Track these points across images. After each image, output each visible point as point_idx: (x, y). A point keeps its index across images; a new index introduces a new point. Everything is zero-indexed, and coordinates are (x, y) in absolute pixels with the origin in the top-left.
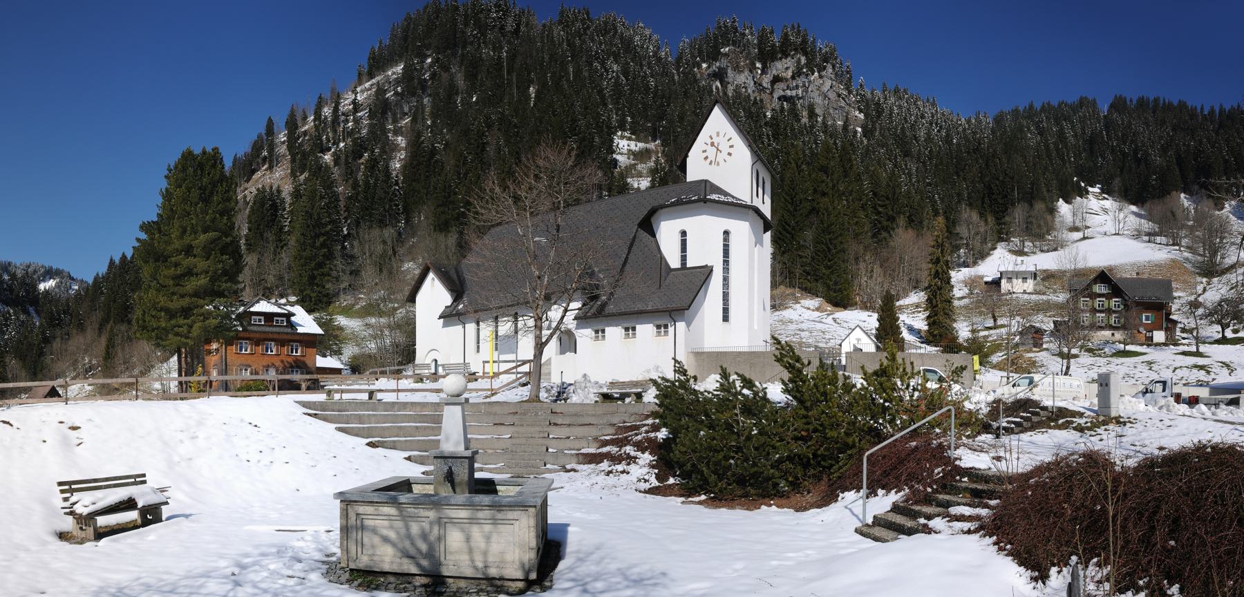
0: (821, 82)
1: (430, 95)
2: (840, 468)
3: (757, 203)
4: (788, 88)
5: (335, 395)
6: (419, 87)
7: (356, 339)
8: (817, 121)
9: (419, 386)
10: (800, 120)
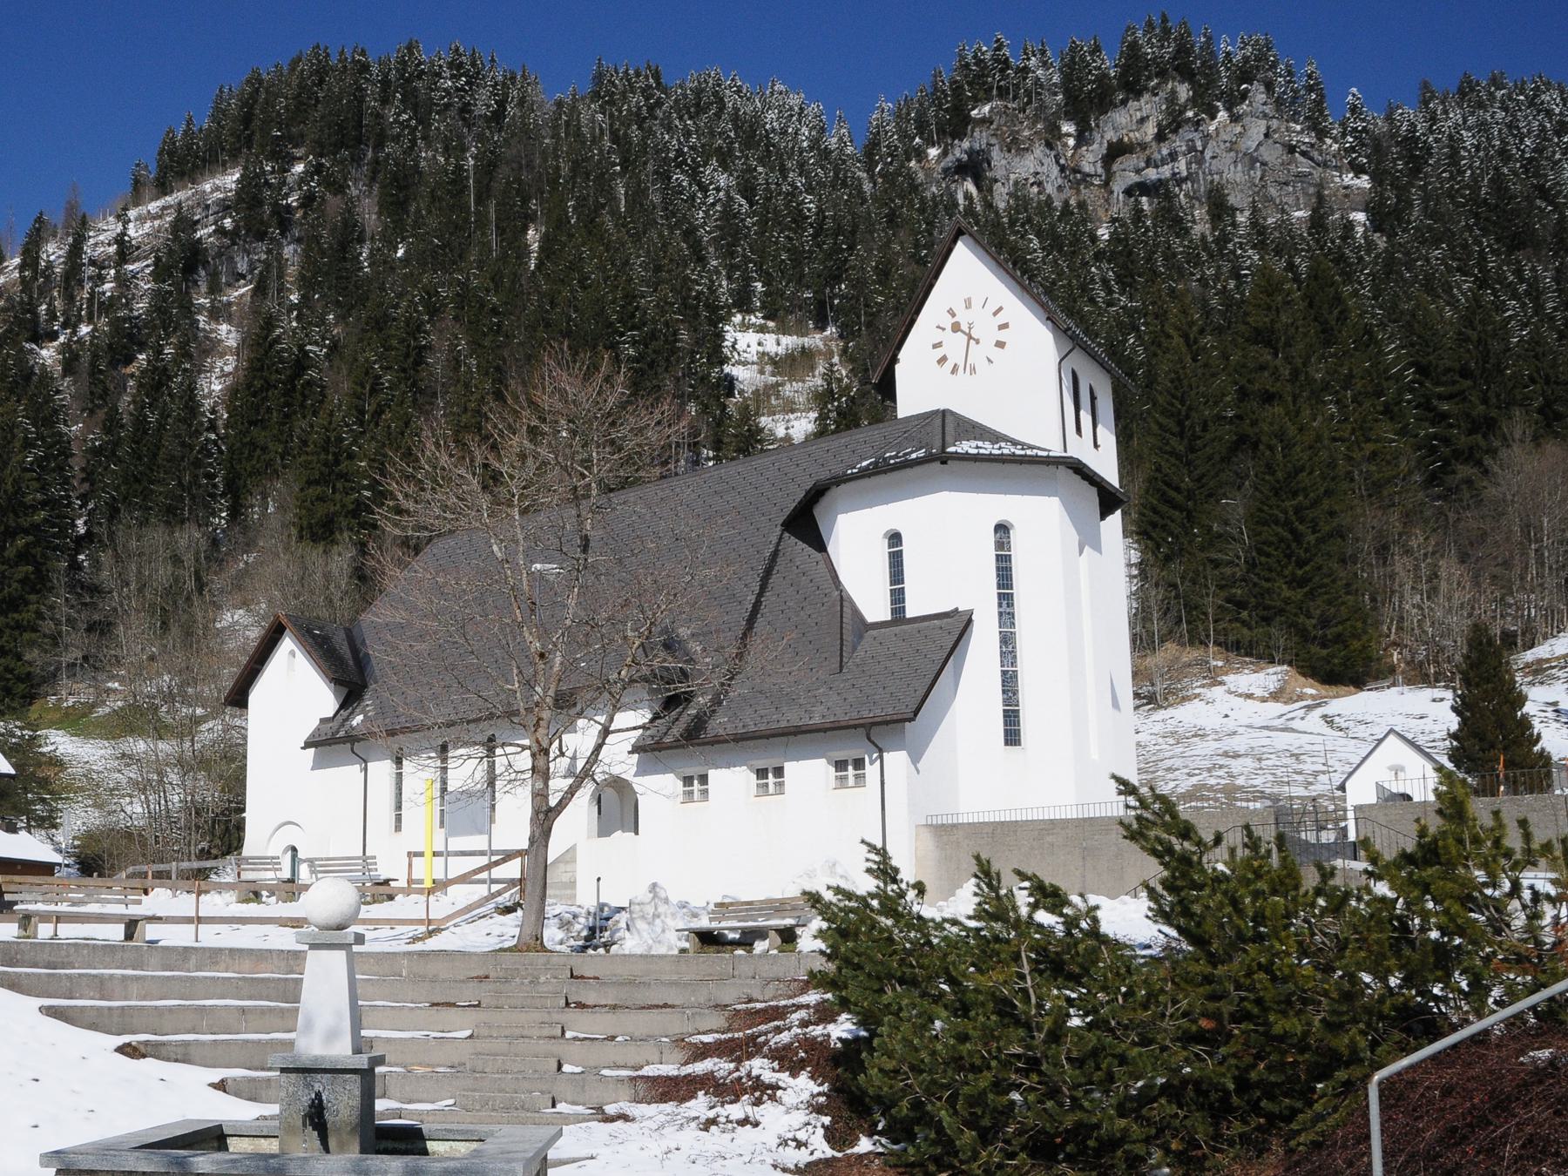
0: (1238, 129)
1: (299, 241)
2: (1319, 1118)
3: (1080, 449)
4: (1149, 163)
5: (41, 926)
6: (275, 221)
7: (95, 790)
8: (1234, 225)
9: (252, 909)
10: (1187, 231)
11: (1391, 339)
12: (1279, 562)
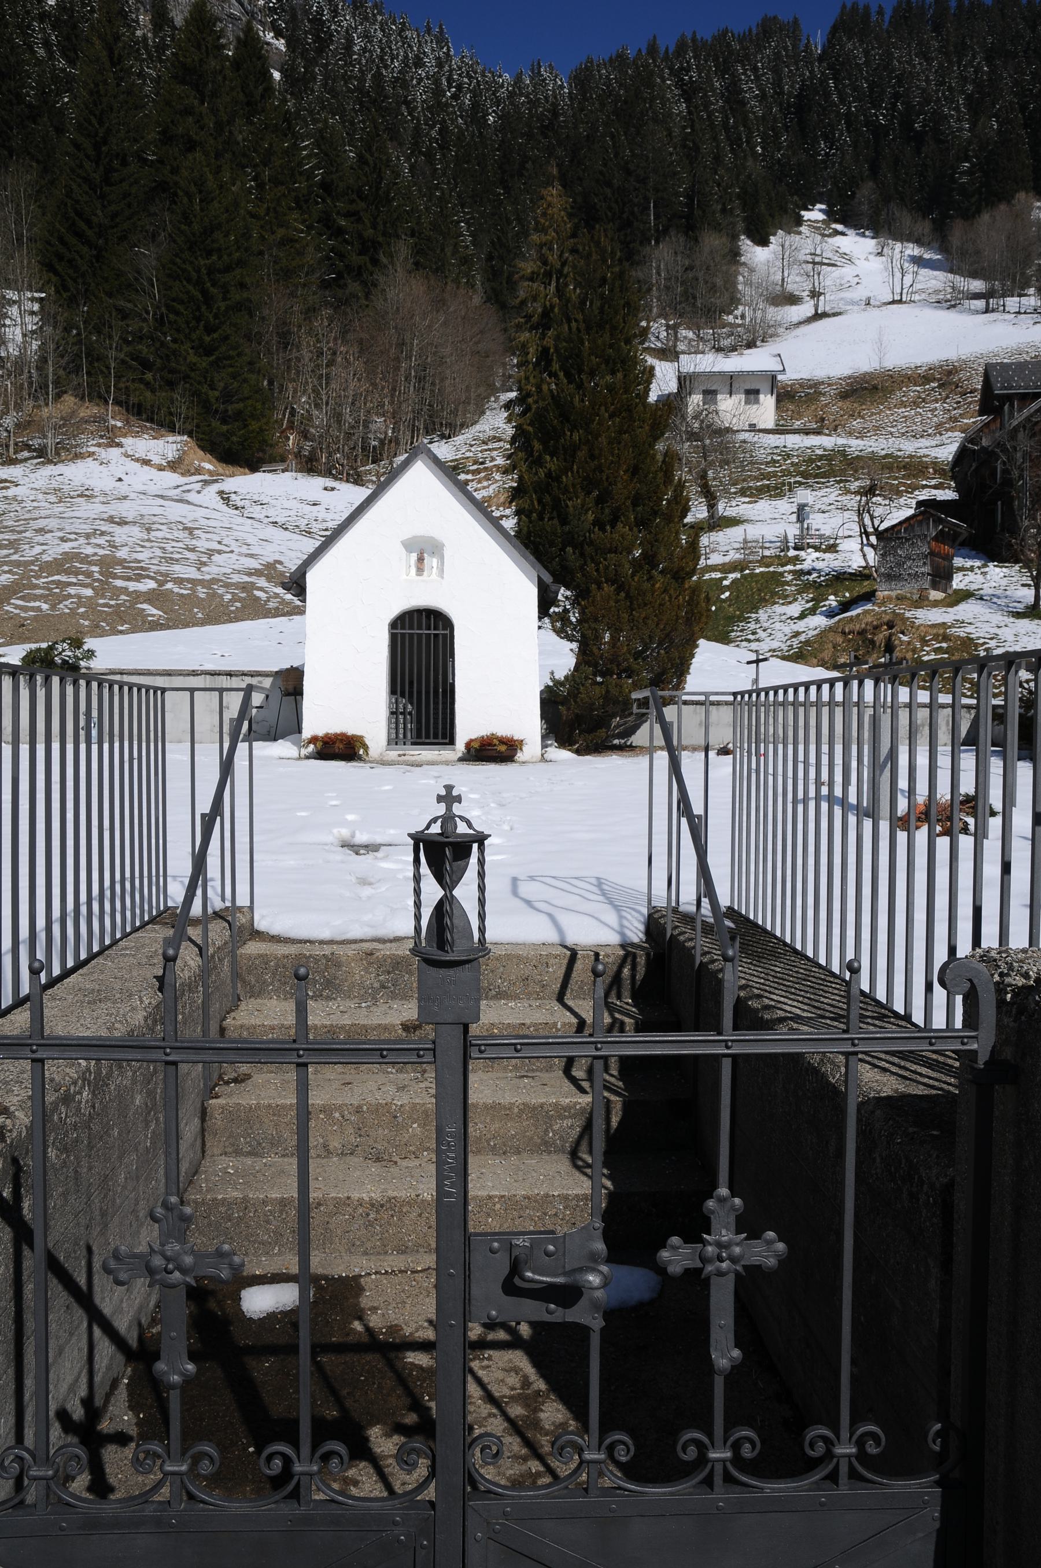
11: (308, 136)
12: (187, 323)
